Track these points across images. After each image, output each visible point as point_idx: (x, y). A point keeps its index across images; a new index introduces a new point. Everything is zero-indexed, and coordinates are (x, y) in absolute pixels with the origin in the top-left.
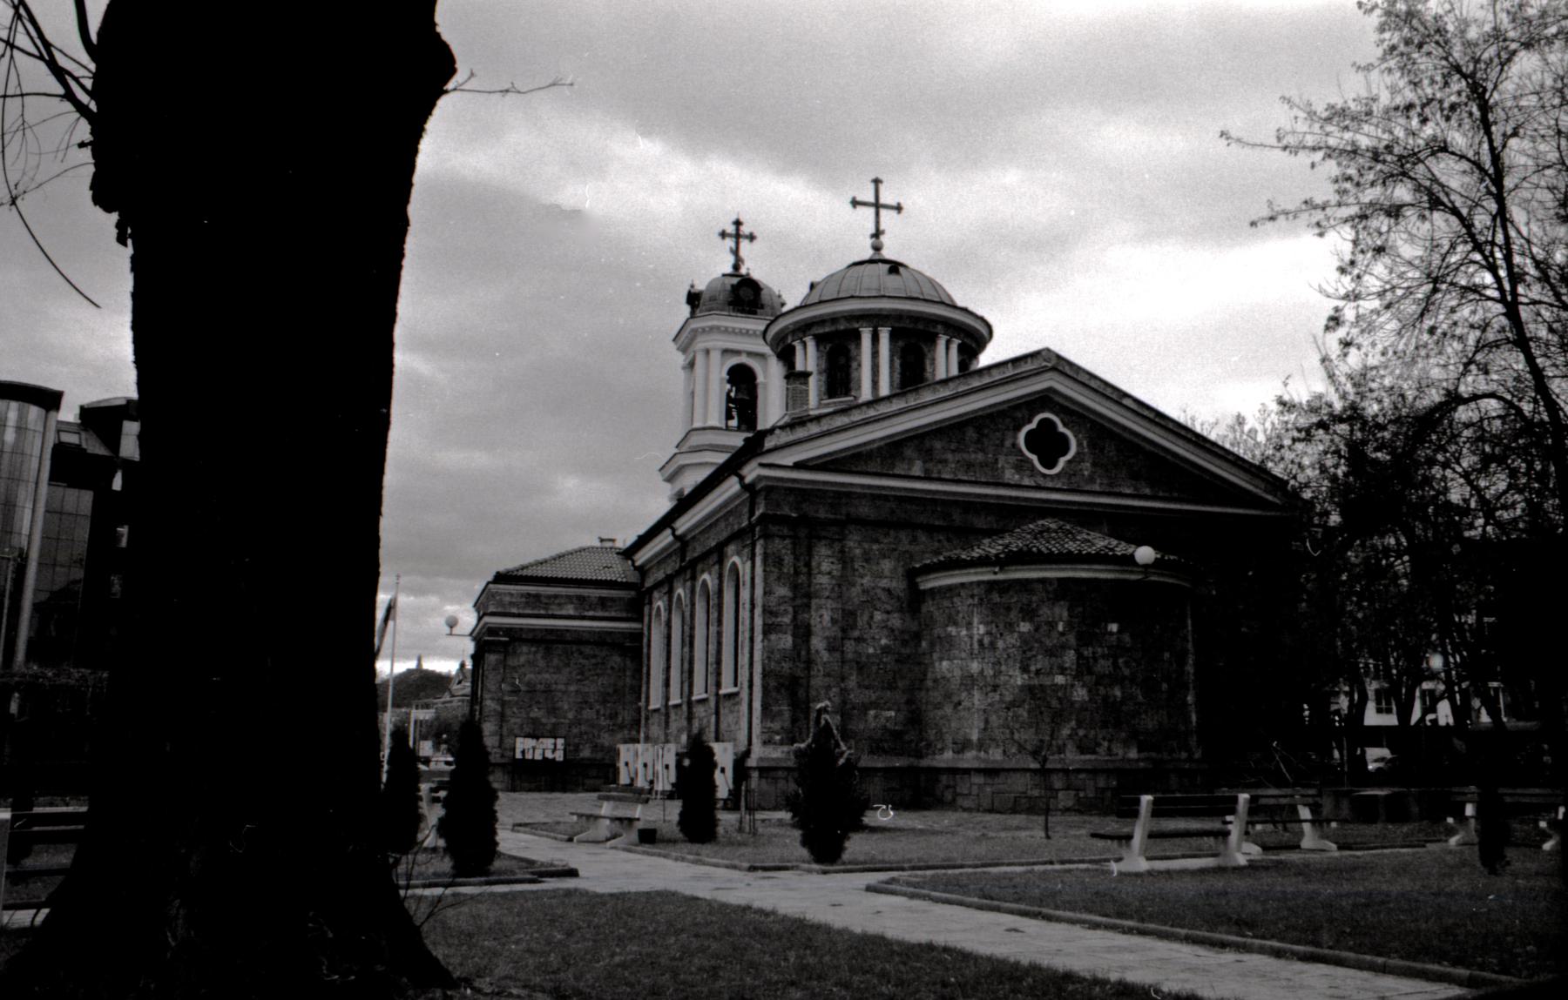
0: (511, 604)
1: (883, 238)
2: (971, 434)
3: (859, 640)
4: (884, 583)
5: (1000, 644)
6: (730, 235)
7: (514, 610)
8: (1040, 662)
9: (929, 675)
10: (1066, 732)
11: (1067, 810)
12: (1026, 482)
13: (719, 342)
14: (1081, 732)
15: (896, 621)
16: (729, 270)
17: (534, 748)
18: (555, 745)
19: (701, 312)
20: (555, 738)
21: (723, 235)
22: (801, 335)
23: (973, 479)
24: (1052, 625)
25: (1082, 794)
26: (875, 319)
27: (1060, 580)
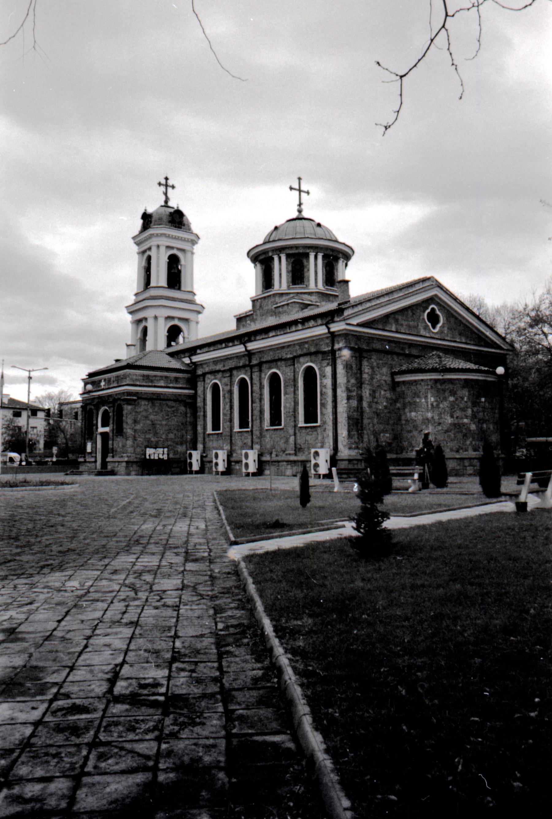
0: (136, 380)
1: (303, 207)
2: (410, 313)
3: (377, 403)
4: (384, 378)
5: (441, 406)
6: (163, 185)
7: (138, 383)
8: (458, 413)
9: (403, 417)
10: (468, 442)
11: (470, 475)
12: (428, 335)
13: (164, 242)
14: (474, 443)
15: (388, 395)
16: (163, 204)
17: (154, 453)
18: (163, 451)
19: (155, 225)
20: (164, 448)
22: (278, 253)
24: (462, 398)
25: (475, 468)
26: (316, 248)
27: (466, 380)
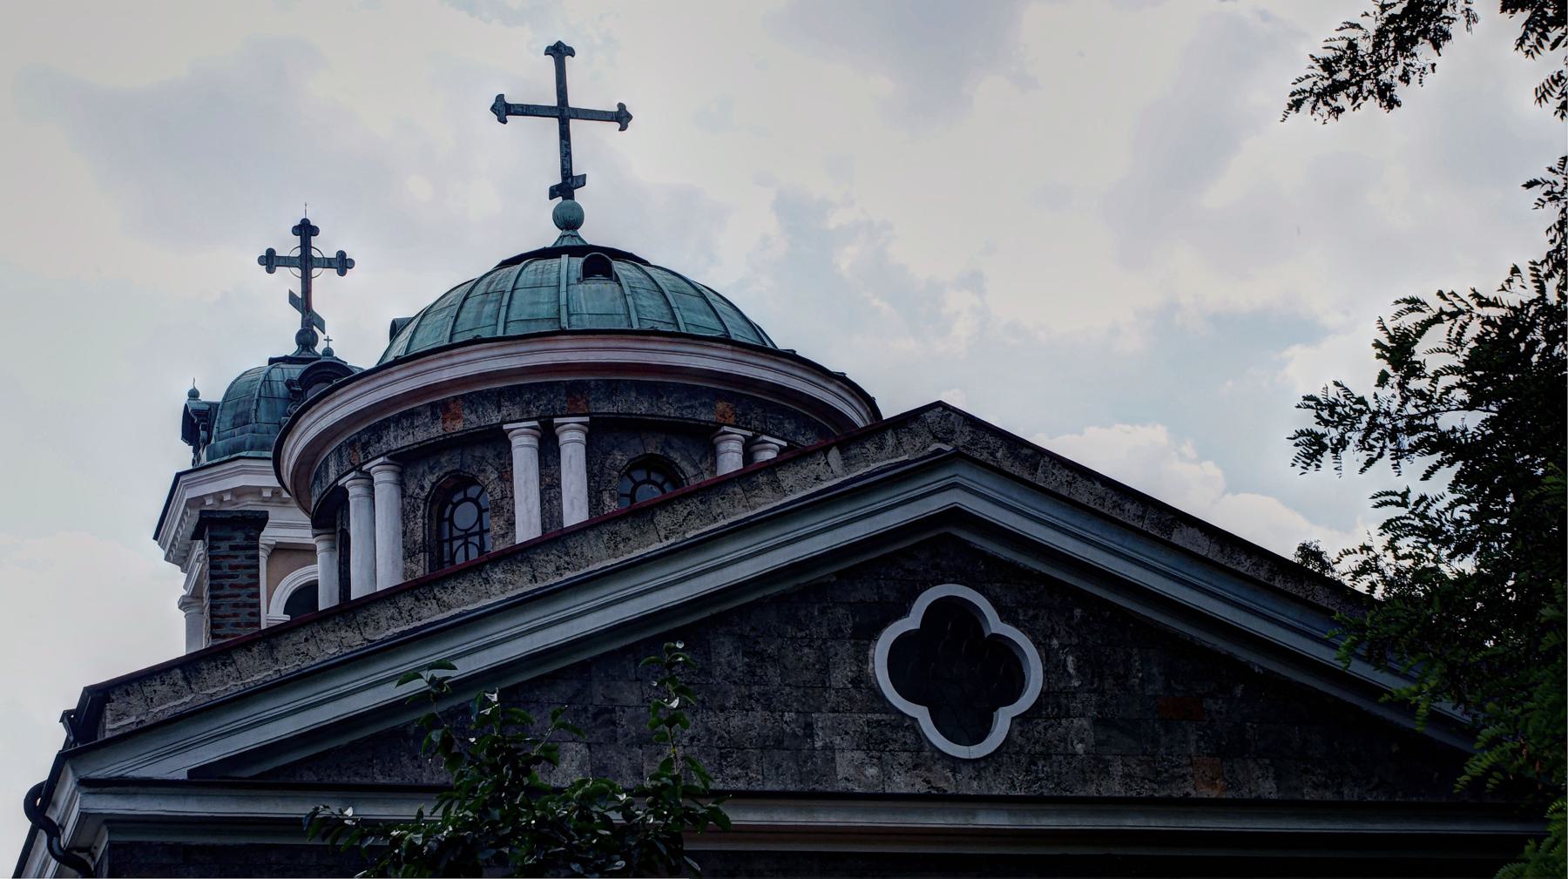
2: (726, 652)
6: (287, 262)
12: (901, 783)
16: (291, 348)
21: (270, 261)
23: (741, 785)
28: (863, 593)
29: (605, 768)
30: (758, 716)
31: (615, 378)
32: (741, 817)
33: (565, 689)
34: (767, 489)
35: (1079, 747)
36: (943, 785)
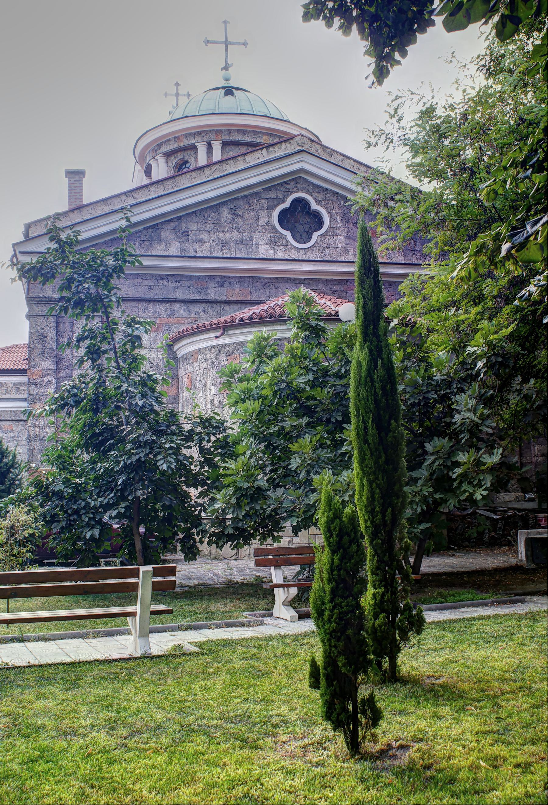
12: (280, 255)
28: (272, 195)
29: (185, 249)
30: (235, 234)
31: (230, 129)
32: (146, 262)
33: (173, 225)
34: (242, 162)
35: (340, 246)
36: (294, 256)
